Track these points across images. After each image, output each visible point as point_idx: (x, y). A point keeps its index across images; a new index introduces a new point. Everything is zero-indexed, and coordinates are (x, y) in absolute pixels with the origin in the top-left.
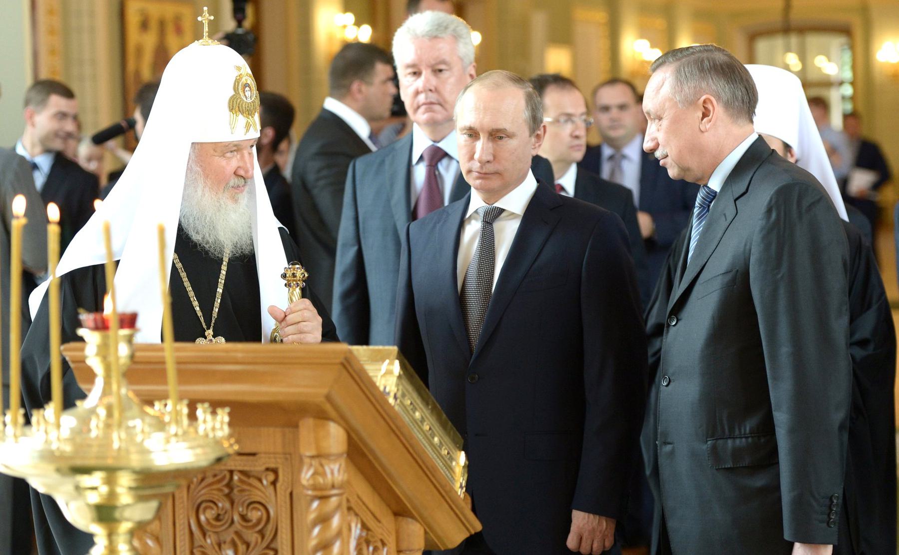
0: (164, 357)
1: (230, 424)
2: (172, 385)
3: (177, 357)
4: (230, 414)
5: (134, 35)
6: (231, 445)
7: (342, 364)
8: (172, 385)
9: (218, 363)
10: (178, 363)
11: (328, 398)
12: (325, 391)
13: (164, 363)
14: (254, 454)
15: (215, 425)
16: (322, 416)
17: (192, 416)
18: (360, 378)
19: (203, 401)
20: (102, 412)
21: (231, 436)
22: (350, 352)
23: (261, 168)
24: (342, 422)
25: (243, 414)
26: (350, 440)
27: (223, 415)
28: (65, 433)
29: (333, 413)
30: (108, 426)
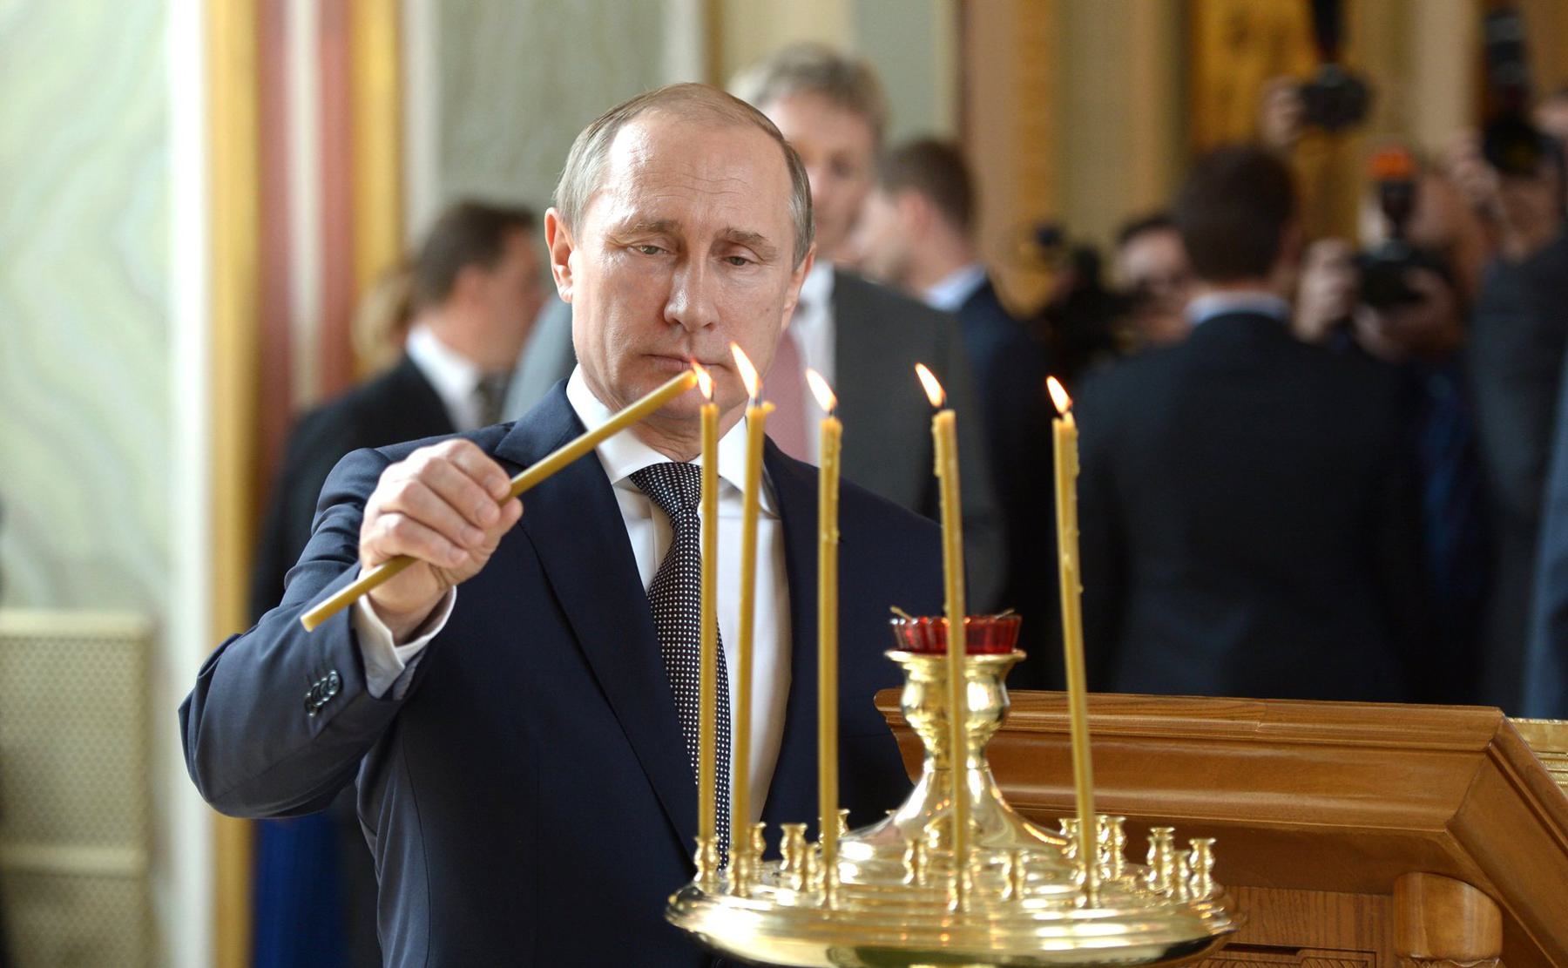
0: (1067, 724)
1: (1215, 874)
2: (1081, 788)
3: (1093, 725)
4: (1213, 849)
5: (1217, 61)
6: (1215, 917)
7: (1487, 752)
8: (1081, 788)
9: (1213, 741)
10: (1093, 736)
11: (1454, 827)
12: (1449, 813)
13: (1066, 735)
14: (1293, 951)
15: (1187, 877)
16: (1446, 871)
17: (1135, 853)
18: (1527, 784)
19: (1163, 823)
20: (932, 835)
21: (1215, 899)
22: (1507, 726)
23: (754, 363)
24: (1488, 885)
25: (1245, 855)
26: (1509, 929)
27: (1202, 854)
28: (847, 872)
29: (1468, 864)
30: (940, 862)
